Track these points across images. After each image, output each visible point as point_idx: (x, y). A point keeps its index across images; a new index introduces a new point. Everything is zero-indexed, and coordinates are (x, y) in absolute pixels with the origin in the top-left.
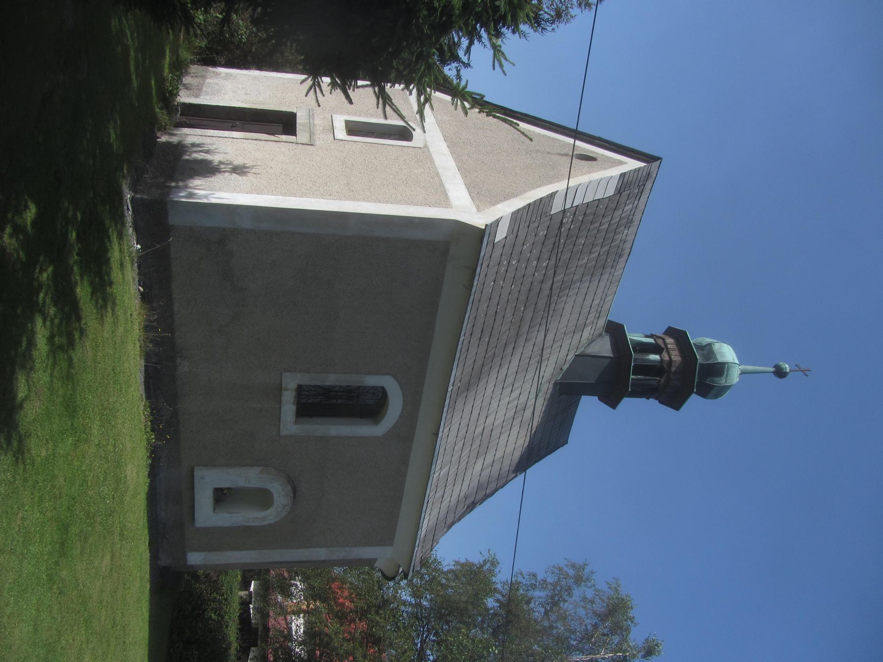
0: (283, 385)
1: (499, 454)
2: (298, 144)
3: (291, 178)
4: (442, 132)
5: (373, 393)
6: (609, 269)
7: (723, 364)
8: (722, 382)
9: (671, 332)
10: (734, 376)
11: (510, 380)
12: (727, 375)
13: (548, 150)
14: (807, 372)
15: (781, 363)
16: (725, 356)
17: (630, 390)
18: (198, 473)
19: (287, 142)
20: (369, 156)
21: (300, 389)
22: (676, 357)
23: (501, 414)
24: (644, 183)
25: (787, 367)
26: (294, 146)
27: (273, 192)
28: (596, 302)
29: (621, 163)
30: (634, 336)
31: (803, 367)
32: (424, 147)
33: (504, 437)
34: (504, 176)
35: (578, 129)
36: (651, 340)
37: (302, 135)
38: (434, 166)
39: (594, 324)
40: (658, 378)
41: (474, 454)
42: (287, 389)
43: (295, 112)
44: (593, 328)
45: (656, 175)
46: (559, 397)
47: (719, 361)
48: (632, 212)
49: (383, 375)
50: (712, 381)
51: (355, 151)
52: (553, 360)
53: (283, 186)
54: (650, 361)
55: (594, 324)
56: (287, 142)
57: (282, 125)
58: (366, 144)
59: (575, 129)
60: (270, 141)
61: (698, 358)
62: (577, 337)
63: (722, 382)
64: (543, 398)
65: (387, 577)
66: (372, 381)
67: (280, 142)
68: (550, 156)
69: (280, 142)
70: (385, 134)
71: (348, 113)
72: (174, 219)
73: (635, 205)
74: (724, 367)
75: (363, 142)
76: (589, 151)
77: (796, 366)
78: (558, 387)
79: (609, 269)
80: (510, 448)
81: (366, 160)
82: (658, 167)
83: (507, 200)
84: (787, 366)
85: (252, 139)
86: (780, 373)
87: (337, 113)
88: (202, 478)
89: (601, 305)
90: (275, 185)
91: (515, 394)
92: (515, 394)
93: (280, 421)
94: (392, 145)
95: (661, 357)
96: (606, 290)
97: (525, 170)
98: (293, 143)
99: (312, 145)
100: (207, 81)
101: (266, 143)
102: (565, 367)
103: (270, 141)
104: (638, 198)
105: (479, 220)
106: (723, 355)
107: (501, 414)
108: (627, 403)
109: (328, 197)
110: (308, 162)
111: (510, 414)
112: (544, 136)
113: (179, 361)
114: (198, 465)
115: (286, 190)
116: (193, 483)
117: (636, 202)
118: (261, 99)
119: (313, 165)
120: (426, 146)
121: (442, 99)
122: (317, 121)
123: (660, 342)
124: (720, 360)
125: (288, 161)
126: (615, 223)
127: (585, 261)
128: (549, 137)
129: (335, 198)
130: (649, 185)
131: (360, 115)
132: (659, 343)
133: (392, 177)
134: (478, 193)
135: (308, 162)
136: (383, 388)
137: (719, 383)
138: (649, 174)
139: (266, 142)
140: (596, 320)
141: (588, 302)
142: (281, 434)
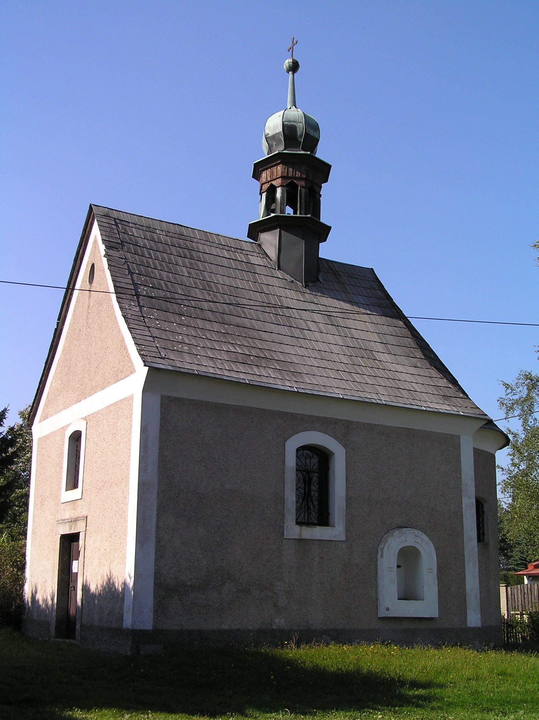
0: (297, 537)
1: (375, 337)
2: (86, 529)
3: (113, 532)
4: (72, 404)
5: (306, 459)
6: (194, 244)
7: (283, 125)
8: (301, 127)
9: (256, 175)
10: (295, 114)
11: (297, 333)
12: (294, 122)
13: (86, 307)
14: (295, 42)
15: (285, 67)
16: (277, 125)
17: (309, 216)
18: (382, 613)
19: (85, 539)
20: (95, 468)
21: (299, 523)
22: (279, 170)
23: (330, 339)
24: (113, 219)
25: (288, 62)
26: (88, 533)
27: (125, 545)
28: (226, 254)
29: (95, 241)
30: (260, 215)
31: (291, 45)
32: (86, 420)
33: (355, 334)
34: (108, 349)
35: (66, 287)
36: (264, 195)
37: (79, 528)
38: (101, 411)
39: (248, 253)
40: (299, 188)
41: (370, 363)
42: (300, 535)
43: (60, 536)
44: (252, 254)
45: (105, 208)
46: (321, 282)
47: (282, 130)
48: (140, 227)
49: (285, 450)
50: (301, 136)
51: (91, 480)
52: (281, 292)
53: (119, 538)
54: (282, 197)
55: (248, 253)
56: (85, 539)
57: (72, 543)
58: (85, 471)
59: (65, 289)
60: (84, 554)
61: (277, 152)
62: (258, 270)
63: (301, 127)
64: (320, 298)
65: (507, 442)
66: (291, 460)
67: (85, 545)
68: (91, 306)
69: (85, 545)
70: (77, 455)
71: (60, 489)
72: (148, 626)
73: (133, 226)
74: (287, 125)
75: (84, 473)
76: (86, 270)
77: (289, 51)
78: (310, 284)
79: (194, 244)
80: (371, 327)
81: (98, 470)
82: (98, 207)
83: (126, 346)
84: (287, 61)
85: (84, 569)
86: (294, 67)
87: (60, 499)
88: (388, 609)
89: (229, 249)
90: (119, 545)
91: (312, 326)
92: (312, 326)
93: (331, 541)
94: (85, 448)
95: (278, 187)
96: (215, 245)
97: (103, 330)
98: (85, 534)
99: (87, 517)
100: (35, 618)
101: (83, 540)
102: (289, 278)
103: (84, 554)
104: (126, 224)
105: (142, 372)
106: (276, 127)
107: (330, 339)
108: (324, 219)
109: (127, 499)
110: (100, 520)
111: (332, 329)
112: (74, 311)
113: (274, 627)
114: (377, 614)
115: (122, 535)
116: (395, 618)
117: (131, 225)
118: (50, 567)
119: (103, 515)
120: (85, 419)
121: (45, 404)
122: (67, 516)
123: (265, 187)
124: (280, 129)
125: (100, 537)
126: (149, 243)
127: (184, 269)
128: (75, 306)
129: (127, 494)
130: (115, 215)
131: (61, 478)
132: (266, 188)
133: (110, 447)
134: (121, 372)
135: (100, 520)
136: (298, 450)
137: (302, 127)
138: (105, 216)
139: (85, 558)
140: (244, 252)
141: (225, 262)
142: (344, 540)
